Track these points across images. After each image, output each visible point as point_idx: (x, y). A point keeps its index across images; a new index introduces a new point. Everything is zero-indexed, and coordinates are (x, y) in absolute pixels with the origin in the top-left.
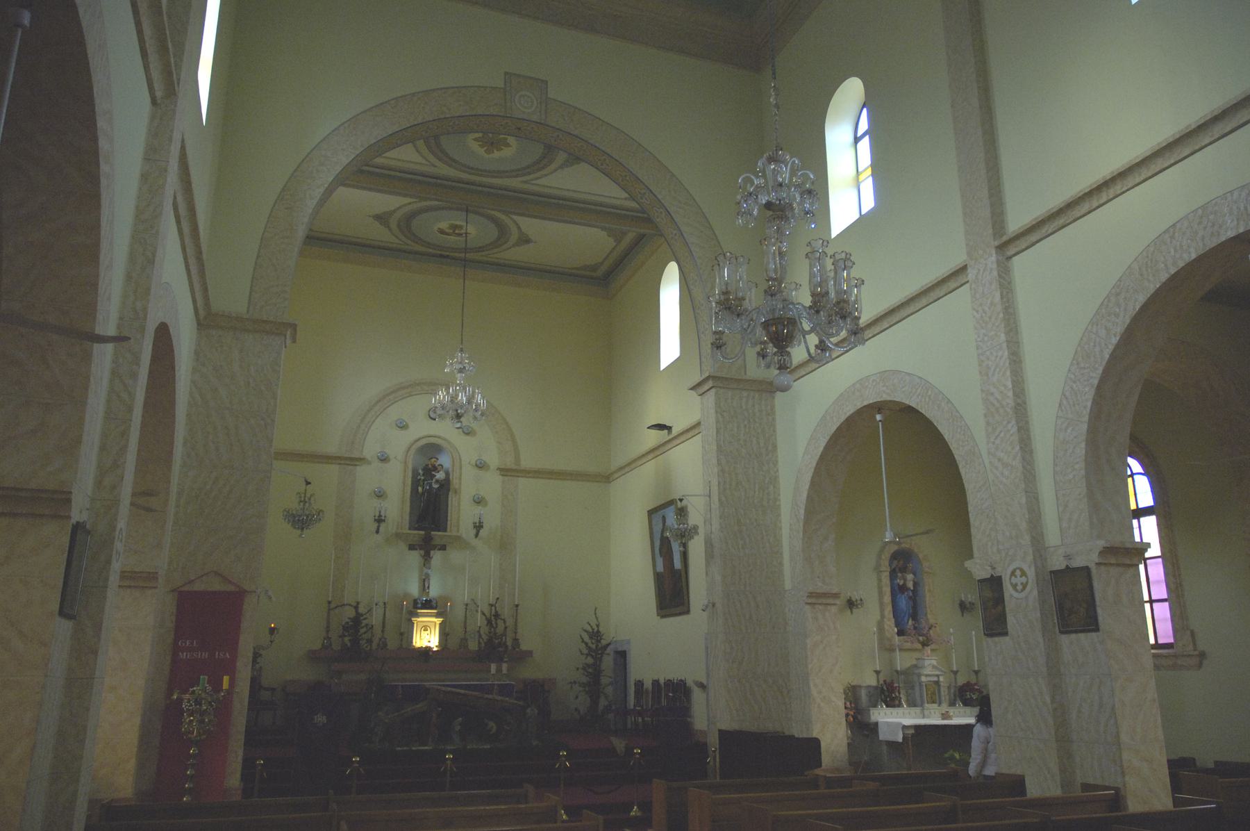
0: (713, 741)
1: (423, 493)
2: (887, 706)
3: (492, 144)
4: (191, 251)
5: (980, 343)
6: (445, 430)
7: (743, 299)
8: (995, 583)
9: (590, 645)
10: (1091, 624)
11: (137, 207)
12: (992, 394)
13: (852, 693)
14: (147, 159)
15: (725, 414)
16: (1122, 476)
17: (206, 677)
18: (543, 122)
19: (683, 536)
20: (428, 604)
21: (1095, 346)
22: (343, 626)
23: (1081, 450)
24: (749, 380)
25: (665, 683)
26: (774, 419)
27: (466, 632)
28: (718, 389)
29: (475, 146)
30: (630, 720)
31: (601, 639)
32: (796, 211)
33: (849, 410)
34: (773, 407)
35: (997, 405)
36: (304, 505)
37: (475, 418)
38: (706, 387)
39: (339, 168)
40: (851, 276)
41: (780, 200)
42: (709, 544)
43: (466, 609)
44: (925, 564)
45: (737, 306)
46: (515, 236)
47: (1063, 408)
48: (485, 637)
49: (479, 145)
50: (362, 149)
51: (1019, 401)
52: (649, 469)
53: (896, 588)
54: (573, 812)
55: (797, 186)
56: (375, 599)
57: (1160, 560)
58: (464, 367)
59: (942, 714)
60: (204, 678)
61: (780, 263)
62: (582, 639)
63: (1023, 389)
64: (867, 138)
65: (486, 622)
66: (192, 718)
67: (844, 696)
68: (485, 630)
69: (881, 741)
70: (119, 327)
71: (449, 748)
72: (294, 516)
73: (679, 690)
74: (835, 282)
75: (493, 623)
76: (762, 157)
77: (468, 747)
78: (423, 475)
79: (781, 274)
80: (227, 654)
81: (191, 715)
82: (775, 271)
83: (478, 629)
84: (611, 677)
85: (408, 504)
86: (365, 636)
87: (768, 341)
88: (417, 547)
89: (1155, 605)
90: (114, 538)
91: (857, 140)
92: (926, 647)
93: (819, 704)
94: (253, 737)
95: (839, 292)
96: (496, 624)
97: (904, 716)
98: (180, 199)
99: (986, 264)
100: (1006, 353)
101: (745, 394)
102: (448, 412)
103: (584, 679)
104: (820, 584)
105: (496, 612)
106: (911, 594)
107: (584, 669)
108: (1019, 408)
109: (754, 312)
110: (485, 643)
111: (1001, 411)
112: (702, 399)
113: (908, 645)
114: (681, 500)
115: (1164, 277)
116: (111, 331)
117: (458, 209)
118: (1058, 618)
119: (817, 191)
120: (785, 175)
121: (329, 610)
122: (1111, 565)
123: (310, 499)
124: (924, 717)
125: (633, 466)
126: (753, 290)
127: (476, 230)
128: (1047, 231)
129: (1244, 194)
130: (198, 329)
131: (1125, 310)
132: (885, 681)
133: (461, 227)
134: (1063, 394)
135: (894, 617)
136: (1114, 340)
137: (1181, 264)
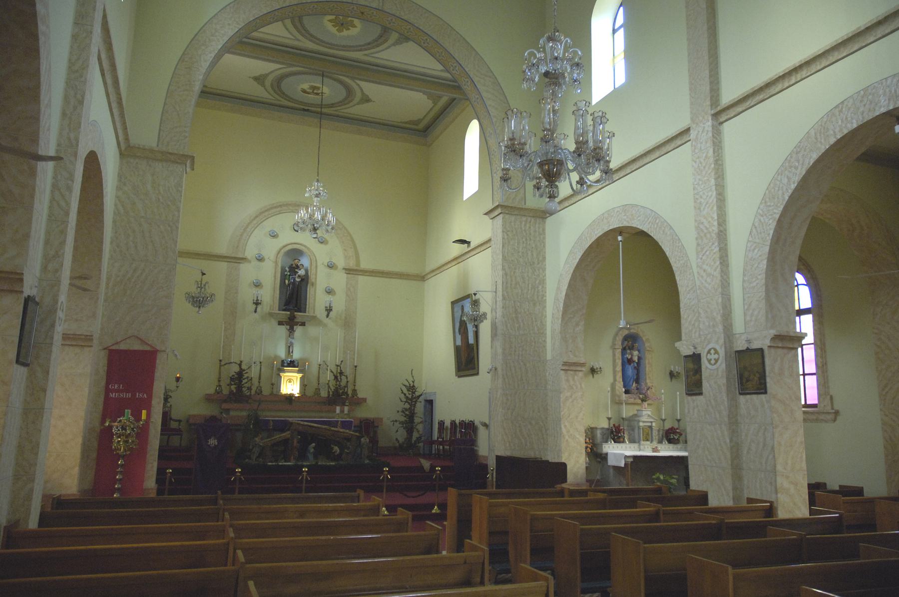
0: (492, 464)
1: (289, 285)
2: (615, 442)
3: (342, 25)
4: (113, 98)
5: (696, 186)
6: (305, 239)
7: (525, 144)
8: (695, 358)
9: (407, 395)
10: (761, 388)
11: (70, 60)
12: (702, 223)
13: (591, 432)
14: (76, 23)
15: (508, 233)
16: (792, 286)
17: (130, 411)
18: (380, 8)
19: (475, 320)
20: (292, 364)
21: (779, 190)
22: (231, 378)
23: (764, 264)
24: (527, 209)
25: (459, 423)
26: (544, 238)
27: (319, 384)
28: (505, 214)
29: (329, 26)
30: (435, 447)
31: (415, 391)
32: (567, 79)
33: (599, 232)
34: (544, 230)
35: (705, 231)
36: (201, 290)
37: (327, 231)
38: (496, 213)
39: (226, 39)
40: (606, 130)
41: (555, 71)
42: (494, 327)
43: (319, 368)
44: (647, 345)
45: (520, 150)
46: (359, 95)
47: (753, 234)
48: (333, 388)
49: (333, 25)
50: (244, 25)
51: (721, 229)
52: (454, 270)
53: (626, 361)
54: (392, 509)
55: (569, 60)
56: (254, 358)
57: (813, 346)
58: (320, 194)
59: (653, 449)
60: (128, 412)
61: (553, 118)
62: (402, 390)
63: (725, 221)
64: (622, 29)
65: (333, 377)
66: (119, 439)
67: (585, 435)
68: (332, 383)
69: (609, 466)
70: (57, 151)
71: (305, 464)
72: (193, 298)
73: (469, 428)
74: (593, 134)
75: (339, 378)
76: (543, 36)
77: (319, 464)
78: (289, 271)
79: (554, 126)
80: (145, 395)
81: (119, 437)
82: (550, 123)
83: (327, 382)
84: (421, 418)
85: (278, 292)
86: (246, 385)
87: (542, 177)
88: (284, 323)
89: (806, 377)
90: (57, 308)
91: (614, 31)
92: (644, 402)
93: (567, 440)
94: (164, 454)
95: (596, 141)
96: (341, 378)
97: (626, 449)
98: (103, 56)
99: (704, 127)
100: (715, 193)
101: (524, 219)
102: (307, 226)
103: (403, 419)
104: (572, 356)
105: (341, 370)
106: (636, 365)
107: (403, 412)
108: (721, 234)
109: (532, 154)
110: (333, 392)
111: (708, 236)
112: (493, 221)
113: (632, 400)
114: (475, 294)
115: (832, 140)
116: (52, 153)
117: (316, 74)
118: (738, 384)
119: (583, 64)
120: (560, 51)
121: (221, 366)
122: (778, 347)
123: (205, 285)
124: (640, 450)
125: (441, 269)
126: (533, 139)
127: (329, 91)
128: (750, 104)
129: (895, 80)
130: (120, 157)
131: (803, 164)
132: (614, 425)
133: (318, 88)
134: (753, 224)
135: (623, 381)
136: (793, 186)
137: (846, 131)
